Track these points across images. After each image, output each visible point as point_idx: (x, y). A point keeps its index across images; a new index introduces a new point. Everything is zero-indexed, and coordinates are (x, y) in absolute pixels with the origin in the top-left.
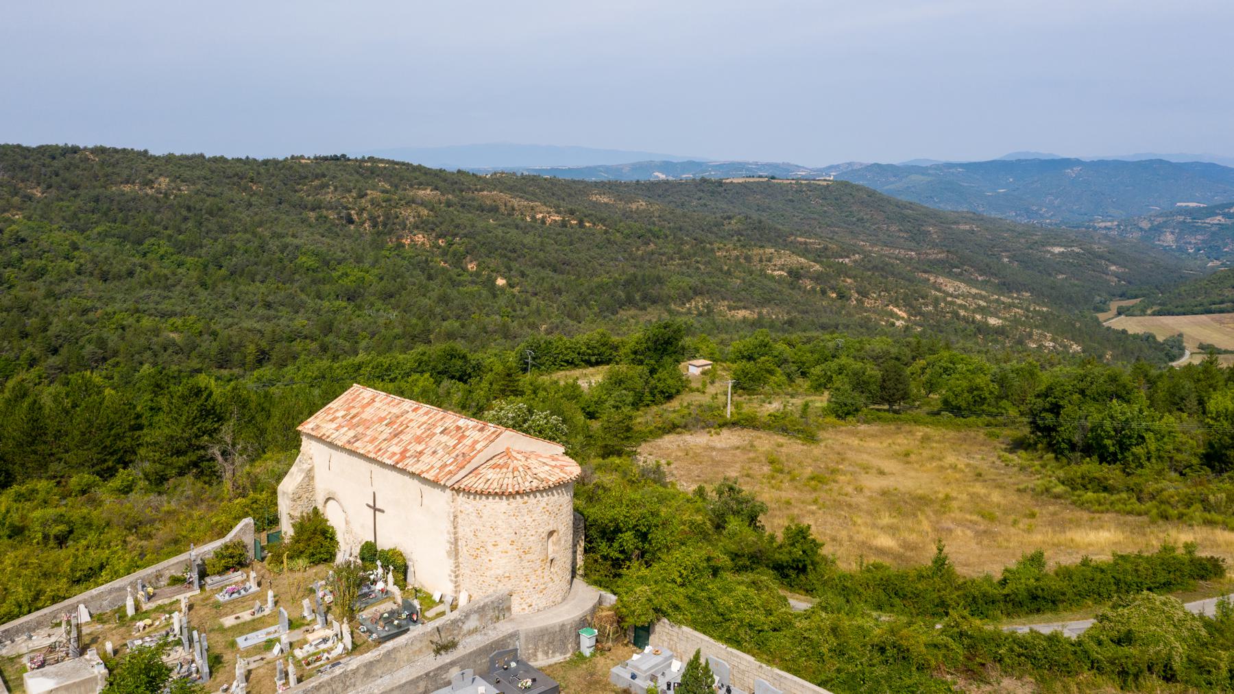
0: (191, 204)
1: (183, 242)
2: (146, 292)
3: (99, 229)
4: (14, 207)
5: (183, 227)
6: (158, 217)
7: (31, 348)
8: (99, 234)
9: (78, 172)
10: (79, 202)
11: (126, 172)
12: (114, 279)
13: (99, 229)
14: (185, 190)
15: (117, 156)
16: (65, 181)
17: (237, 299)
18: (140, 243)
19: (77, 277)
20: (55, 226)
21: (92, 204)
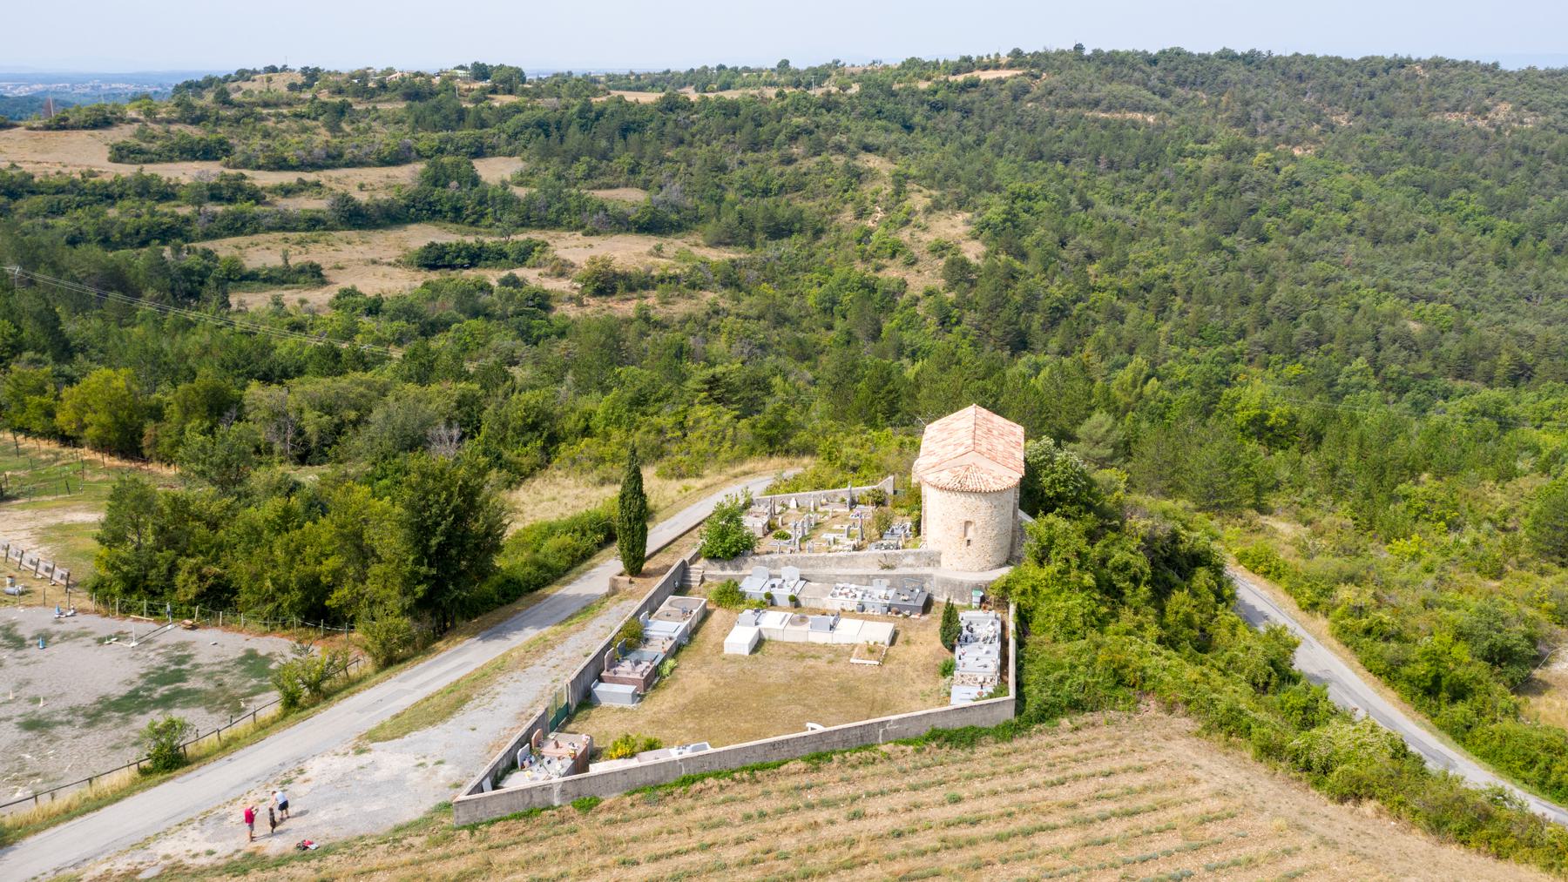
0: (1530, 144)
1: (1501, 198)
2: (1417, 264)
4: (1308, 139)
5: (1510, 176)
6: (1481, 160)
7: (1246, 317)
8: (1397, 179)
9: (1398, 94)
11: (1459, 95)
14: (1530, 122)
15: (1454, 72)
16: (1378, 106)
17: (1539, 287)
19: (1345, 235)
20: (1348, 166)
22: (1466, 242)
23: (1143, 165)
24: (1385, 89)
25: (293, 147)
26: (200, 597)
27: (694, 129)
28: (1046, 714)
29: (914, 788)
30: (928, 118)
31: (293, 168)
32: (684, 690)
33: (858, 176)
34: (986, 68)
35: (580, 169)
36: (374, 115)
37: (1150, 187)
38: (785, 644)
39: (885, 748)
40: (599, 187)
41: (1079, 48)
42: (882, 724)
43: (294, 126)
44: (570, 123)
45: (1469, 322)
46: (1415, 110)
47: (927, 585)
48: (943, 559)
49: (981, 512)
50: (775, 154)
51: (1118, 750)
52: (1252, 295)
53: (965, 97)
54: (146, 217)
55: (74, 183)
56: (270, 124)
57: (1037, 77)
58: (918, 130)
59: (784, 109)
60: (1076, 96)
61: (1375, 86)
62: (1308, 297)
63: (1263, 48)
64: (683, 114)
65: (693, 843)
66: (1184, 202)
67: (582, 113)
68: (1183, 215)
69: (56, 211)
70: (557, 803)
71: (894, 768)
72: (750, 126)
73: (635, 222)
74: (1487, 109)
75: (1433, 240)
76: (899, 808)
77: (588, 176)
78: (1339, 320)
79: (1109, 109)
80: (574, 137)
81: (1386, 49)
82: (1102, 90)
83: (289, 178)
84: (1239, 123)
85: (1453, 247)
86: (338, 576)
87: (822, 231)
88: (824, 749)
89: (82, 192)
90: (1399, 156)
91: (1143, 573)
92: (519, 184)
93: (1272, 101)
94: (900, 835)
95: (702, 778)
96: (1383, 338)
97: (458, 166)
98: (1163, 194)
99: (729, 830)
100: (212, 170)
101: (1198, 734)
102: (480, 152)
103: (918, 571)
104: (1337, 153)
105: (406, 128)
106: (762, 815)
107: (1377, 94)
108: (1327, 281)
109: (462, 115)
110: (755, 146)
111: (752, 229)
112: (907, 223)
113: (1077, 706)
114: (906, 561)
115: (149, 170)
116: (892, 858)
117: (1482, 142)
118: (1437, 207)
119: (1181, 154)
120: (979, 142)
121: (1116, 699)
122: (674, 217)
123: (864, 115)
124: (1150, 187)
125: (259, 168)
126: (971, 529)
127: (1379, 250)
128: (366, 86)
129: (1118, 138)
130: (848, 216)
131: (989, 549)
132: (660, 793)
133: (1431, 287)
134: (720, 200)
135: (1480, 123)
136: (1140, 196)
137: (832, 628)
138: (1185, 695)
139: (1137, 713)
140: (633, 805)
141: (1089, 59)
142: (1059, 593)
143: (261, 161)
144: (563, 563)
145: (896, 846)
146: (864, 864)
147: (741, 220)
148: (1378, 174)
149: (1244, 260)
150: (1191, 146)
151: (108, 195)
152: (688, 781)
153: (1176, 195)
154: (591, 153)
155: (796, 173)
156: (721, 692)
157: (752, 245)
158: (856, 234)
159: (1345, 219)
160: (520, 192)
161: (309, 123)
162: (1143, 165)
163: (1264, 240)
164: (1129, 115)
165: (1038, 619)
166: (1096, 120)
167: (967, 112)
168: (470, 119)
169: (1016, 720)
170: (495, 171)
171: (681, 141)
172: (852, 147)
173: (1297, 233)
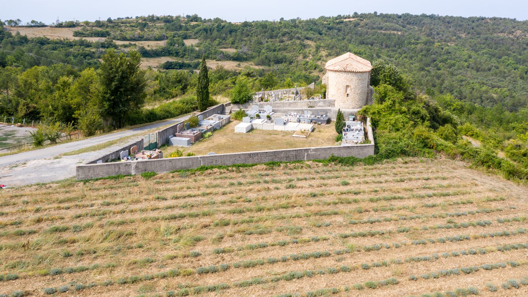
1: (520, 59)
2: (493, 78)
3: (484, 51)
5: (523, 52)
6: (512, 47)
8: (483, 53)
9: (482, 28)
10: (479, 40)
11: (503, 28)
12: (481, 71)
13: (484, 51)
15: (501, 21)
16: (475, 31)
18: (500, 58)
21: (484, 41)
22: (509, 71)
23: (397, 46)
24: (477, 26)
25: (129, 34)
26: (26, 116)
27: (252, 32)
28: (390, 155)
29: (323, 179)
30: (327, 31)
31: (128, 40)
32: (213, 142)
33: (305, 46)
34: (346, 18)
35: (217, 42)
36: (154, 27)
37: (400, 53)
38: (263, 131)
39: (308, 163)
40: (222, 48)
41: (375, 13)
42: (307, 150)
43: (130, 29)
44: (214, 29)
45: (514, 94)
46: (488, 32)
47: (328, 114)
48: (336, 103)
49: (353, 81)
50: (278, 39)
51: (430, 171)
52: (437, 84)
53: (339, 26)
54: (81, 51)
55: (61, 41)
56: (123, 28)
57: (362, 20)
58: (323, 35)
59: (281, 27)
60: (375, 26)
61: (475, 26)
62: (456, 85)
63: (436, 14)
64: (249, 28)
65: (200, 192)
66: (411, 58)
67: (218, 27)
68: (411, 61)
69: (54, 49)
70: (133, 173)
71: (312, 171)
72: (270, 31)
73: (232, 57)
74: (513, 32)
75: (498, 71)
76: (315, 185)
77: (219, 45)
78: (467, 92)
79: (386, 30)
80: (215, 33)
81: (478, 14)
82: (383, 25)
83: (127, 43)
84: (428, 35)
85: (505, 73)
86: (79, 105)
87: (292, 62)
88: (276, 160)
89: (63, 44)
90: (483, 46)
91: (426, 116)
92: (197, 47)
93: (439, 29)
94: (315, 196)
95: (212, 168)
96: (483, 98)
97: (178, 40)
98: (404, 55)
99: (220, 189)
100: (103, 40)
101: (470, 167)
102: (186, 37)
103: (325, 108)
104: (462, 45)
105: (164, 30)
106: (240, 184)
107: (475, 27)
108: (462, 81)
109: (181, 27)
110: (271, 37)
111: (270, 61)
112: (319, 59)
113: (404, 153)
114: (319, 104)
115: (84, 39)
116: (309, 205)
117: (512, 42)
118: (498, 61)
119: (410, 43)
120: (344, 39)
121: (424, 153)
122: (245, 56)
123: (306, 30)
124: (400, 53)
125: (118, 40)
126: (349, 89)
127: (479, 73)
128: (153, 19)
129: (389, 38)
130: (301, 57)
131: (357, 98)
132: (189, 173)
133: (499, 84)
134: (260, 52)
135: (511, 36)
136: (396, 55)
137: (285, 124)
138: (461, 150)
139: (436, 158)
140: (173, 177)
141: (379, 16)
142: (391, 114)
143: (119, 38)
144: (177, 113)
145: (313, 200)
146: (293, 207)
147: (266, 58)
148: (476, 51)
149: (433, 74)
150: (413, 41)
151: (71, 45)
152: (203, 168)
153: (408, 56)
154: (220, 38)
155: (284, 45)
156: (230, 143)
157: (269, 66)
158: (303, 63)
159: (466, 64)
160: (197, 49)
161: (134, 28)
162: (397, 46)
163: (439, 69)
164: (392, 32)
165: (381, 125)
166: (381, 33)
167: (339, 30)
168: (183, 28)
169: (375, 156)
170: (188, 43)
171: (248, 35)
172: (302, 38)
173: (450, 68)
